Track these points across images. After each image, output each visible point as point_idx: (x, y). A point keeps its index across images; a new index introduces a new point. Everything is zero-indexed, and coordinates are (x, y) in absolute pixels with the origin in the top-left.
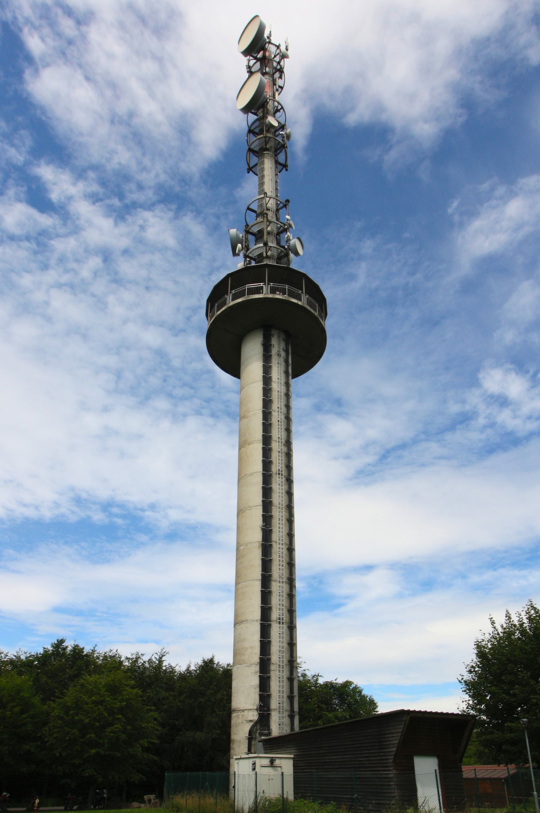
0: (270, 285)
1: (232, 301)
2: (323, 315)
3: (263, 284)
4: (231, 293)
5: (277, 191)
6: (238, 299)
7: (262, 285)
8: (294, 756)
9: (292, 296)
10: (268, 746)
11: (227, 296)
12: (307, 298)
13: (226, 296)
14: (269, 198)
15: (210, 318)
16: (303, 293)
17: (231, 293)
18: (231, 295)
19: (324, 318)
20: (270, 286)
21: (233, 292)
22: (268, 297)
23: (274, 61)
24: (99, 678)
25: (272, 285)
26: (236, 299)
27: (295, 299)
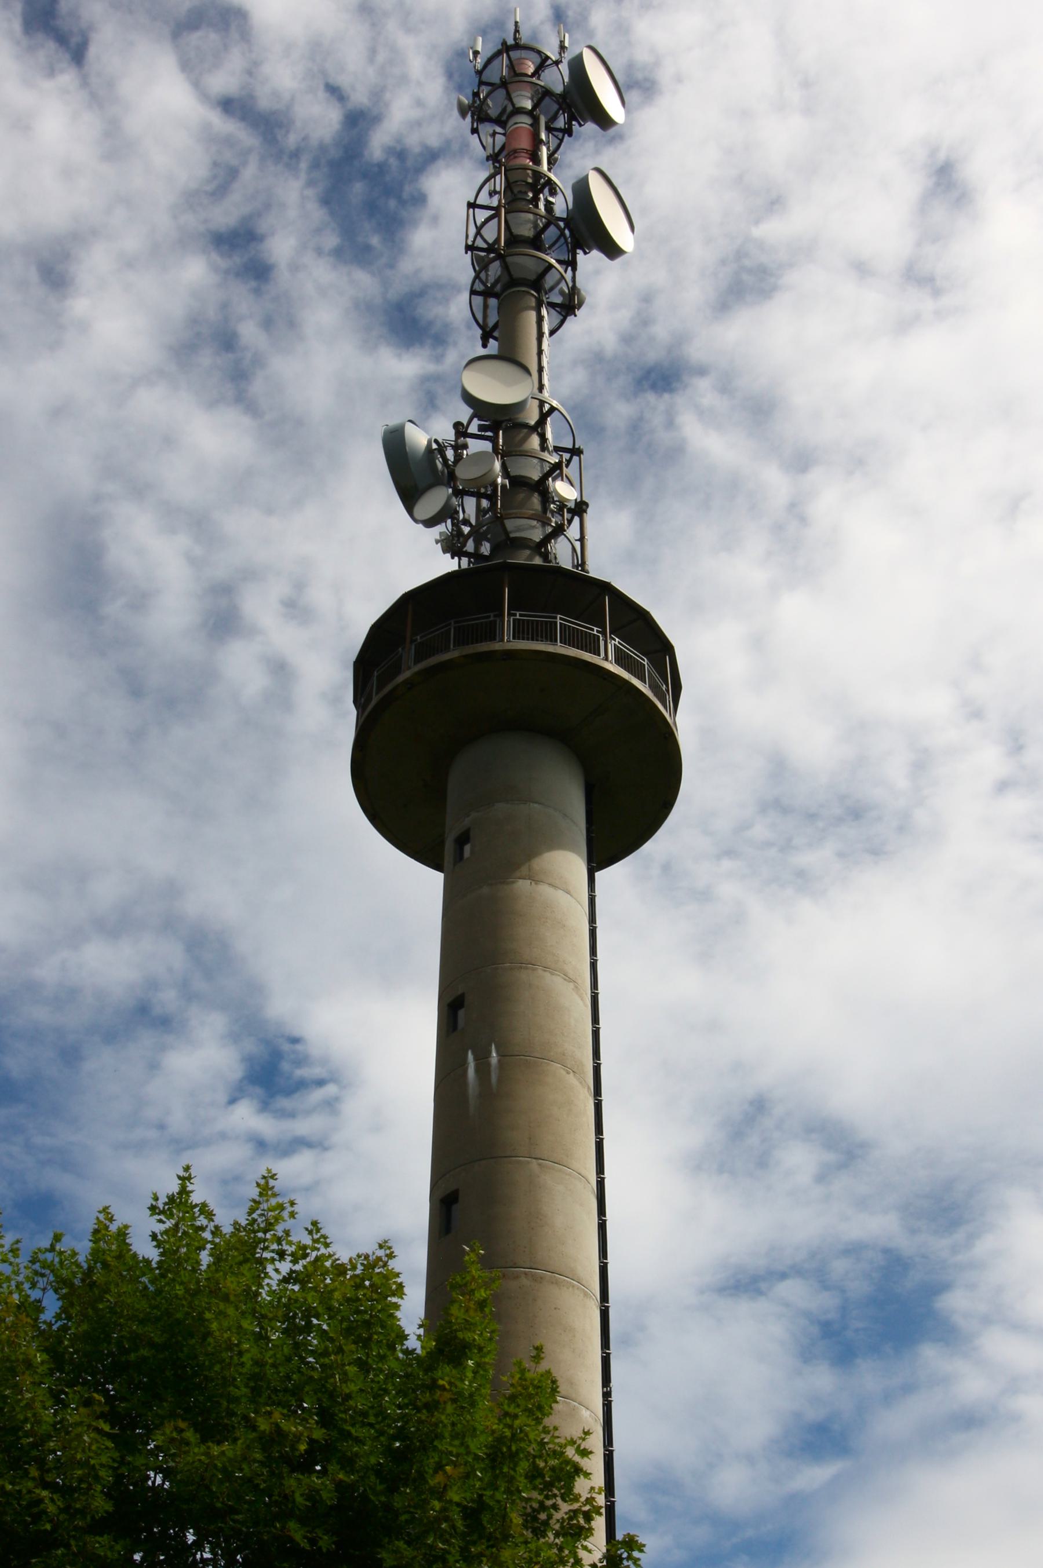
0: (512, 618)
1: (415, 663)
2: (667, 688)
3: (495, 616)
4: (412, 641)
5: (518, 151)
6: (434, 655)
7: (492, 619)
8: (572, 848)
9: (586, 646)
10: (521, 1158)
11: (402, 649)
12: (615, 644)
13: (400, 649)
14: (479, 238)
15: (603, 642)
16: (604, 633)
17: (412, 641)
18: (413, 647)
19: (669, 698)
20: (514, 620)
21: (419, 641)
22: (513, 648)
23: (563, 281)
24: (151, 1332)
25: (518, 617)
26: (430, 656)
27: (638, 679)
